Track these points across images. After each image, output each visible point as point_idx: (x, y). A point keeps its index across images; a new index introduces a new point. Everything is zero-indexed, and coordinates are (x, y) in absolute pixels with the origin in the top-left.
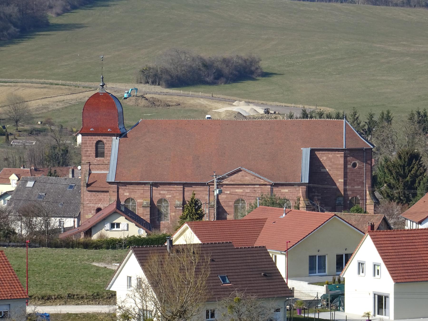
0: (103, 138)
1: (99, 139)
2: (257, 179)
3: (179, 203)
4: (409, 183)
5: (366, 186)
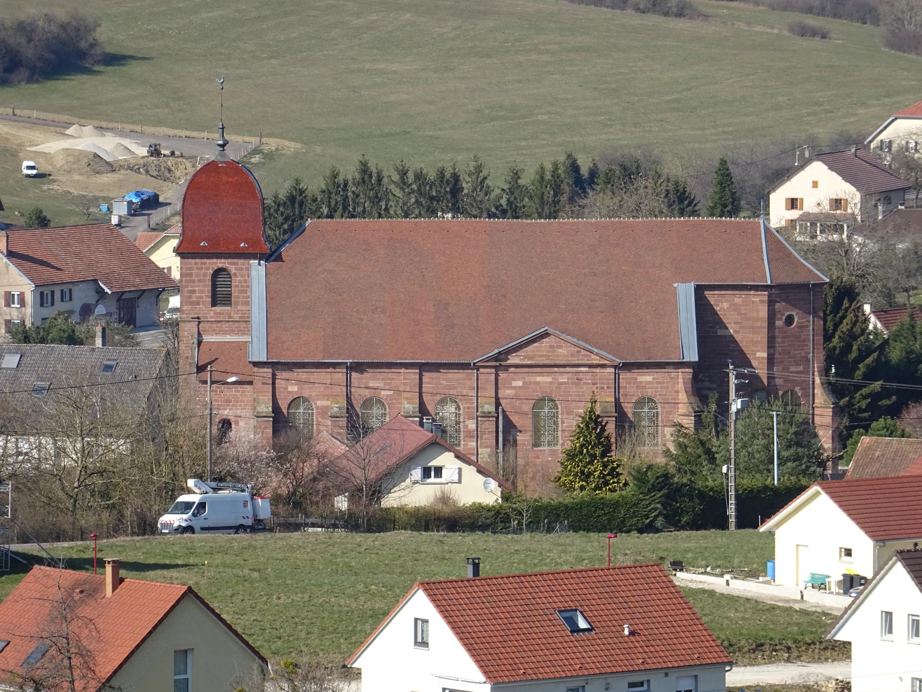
0: (229, 263)
1: (220, 266)
2: (583, 352)
3: (411, 406)
4: (837, 351)
5: (814, 367)
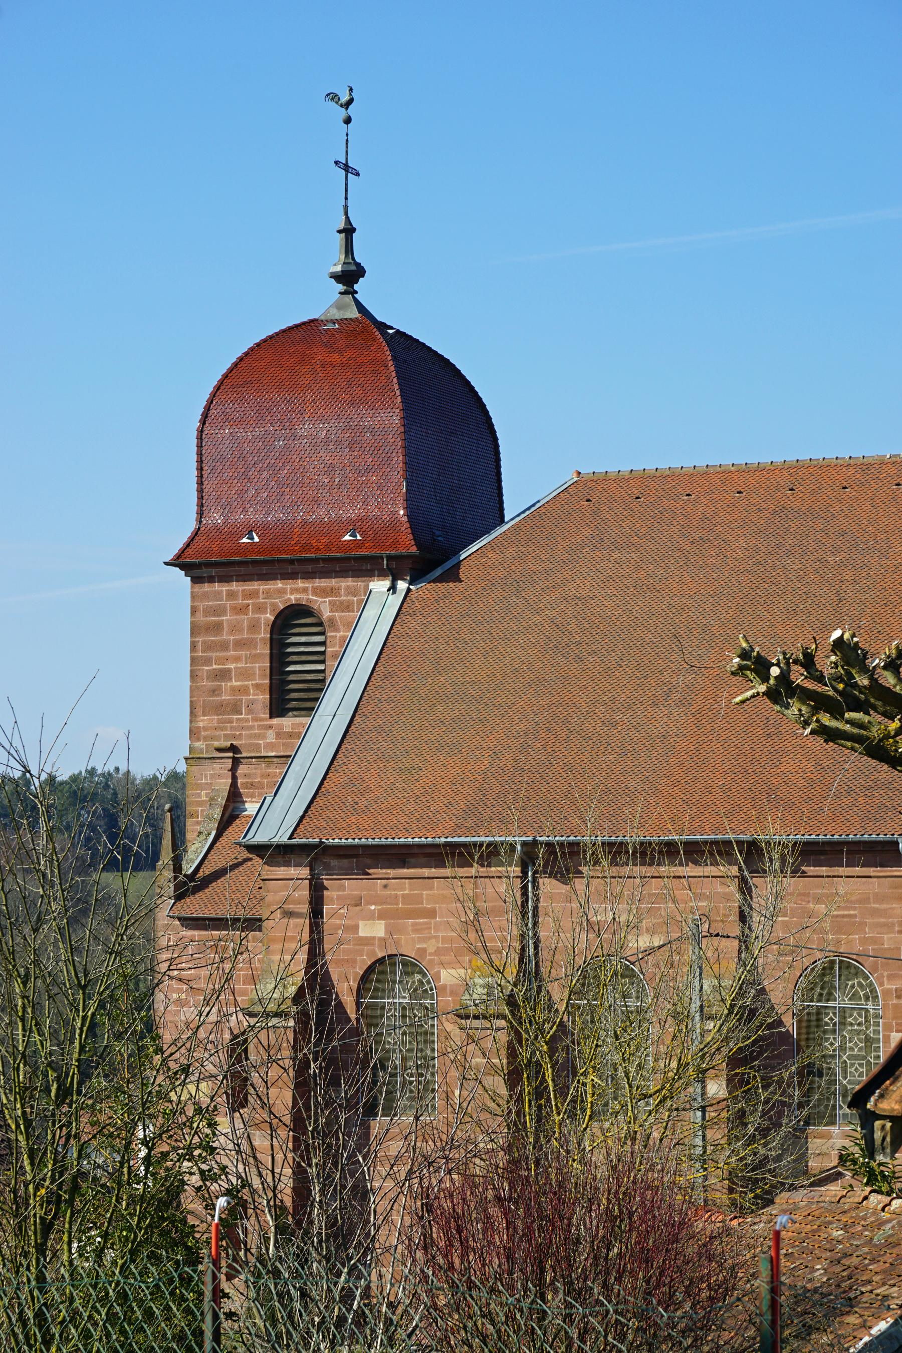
0: (315, 591)
1: (293, 598)
